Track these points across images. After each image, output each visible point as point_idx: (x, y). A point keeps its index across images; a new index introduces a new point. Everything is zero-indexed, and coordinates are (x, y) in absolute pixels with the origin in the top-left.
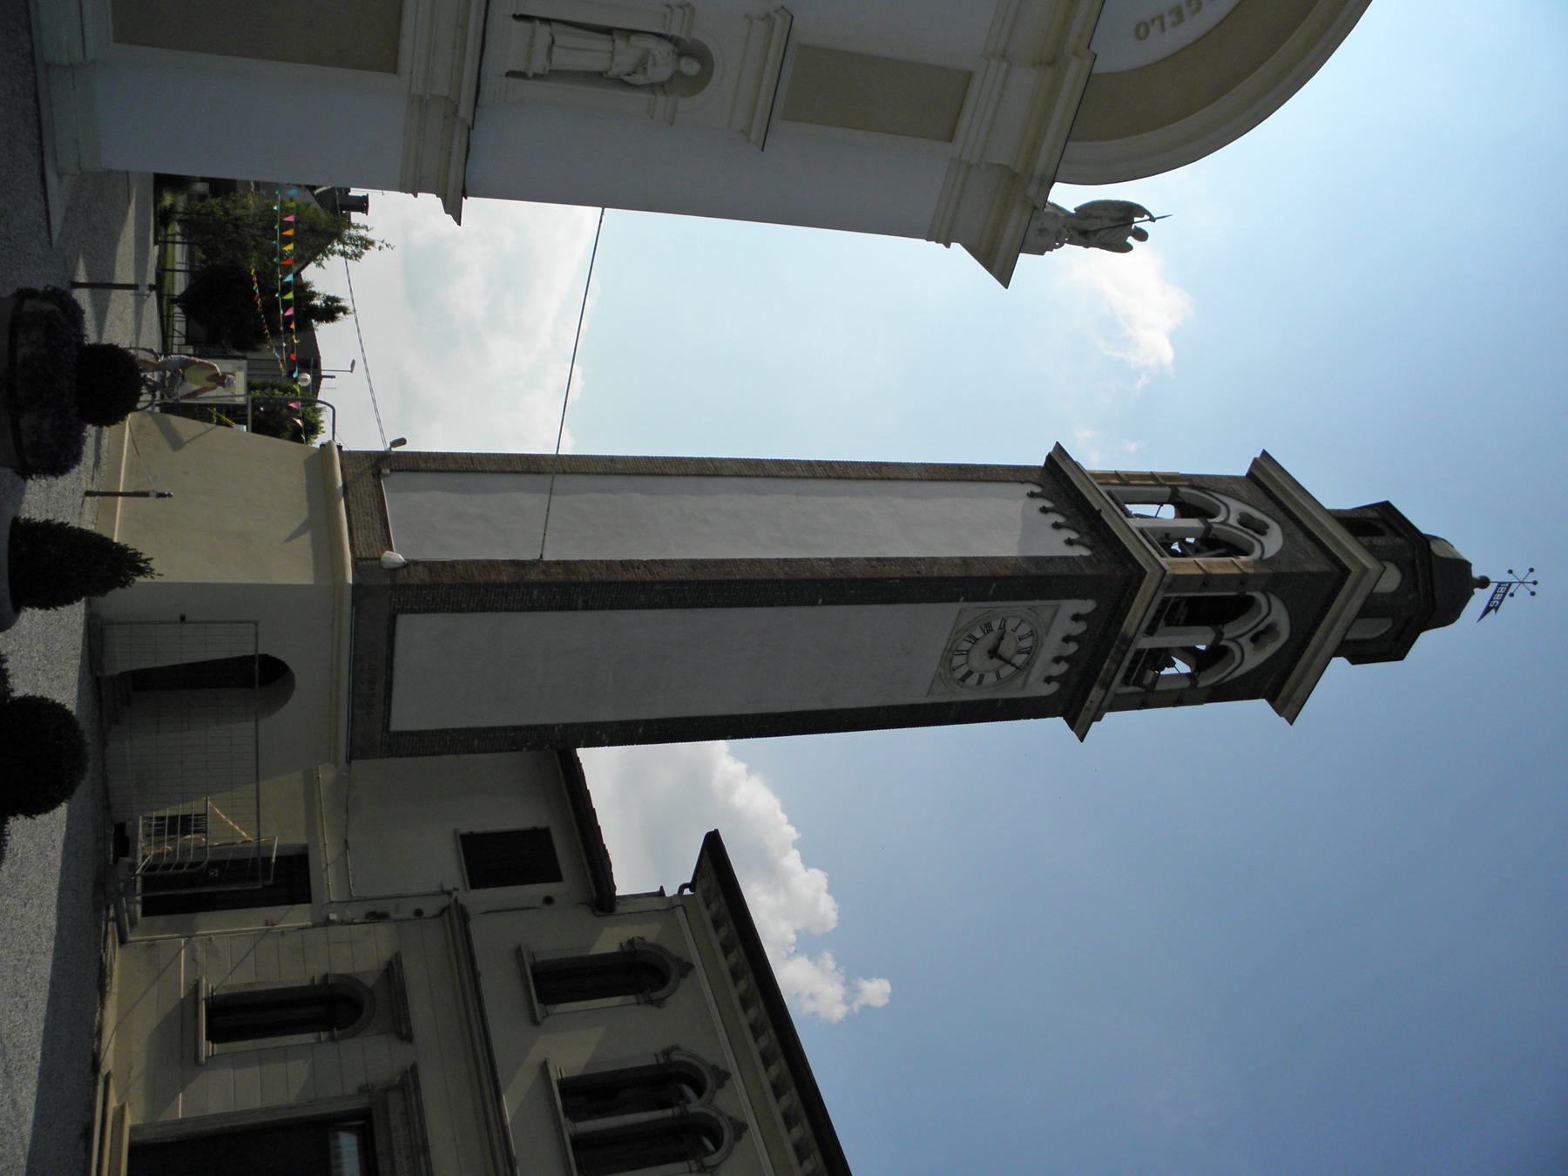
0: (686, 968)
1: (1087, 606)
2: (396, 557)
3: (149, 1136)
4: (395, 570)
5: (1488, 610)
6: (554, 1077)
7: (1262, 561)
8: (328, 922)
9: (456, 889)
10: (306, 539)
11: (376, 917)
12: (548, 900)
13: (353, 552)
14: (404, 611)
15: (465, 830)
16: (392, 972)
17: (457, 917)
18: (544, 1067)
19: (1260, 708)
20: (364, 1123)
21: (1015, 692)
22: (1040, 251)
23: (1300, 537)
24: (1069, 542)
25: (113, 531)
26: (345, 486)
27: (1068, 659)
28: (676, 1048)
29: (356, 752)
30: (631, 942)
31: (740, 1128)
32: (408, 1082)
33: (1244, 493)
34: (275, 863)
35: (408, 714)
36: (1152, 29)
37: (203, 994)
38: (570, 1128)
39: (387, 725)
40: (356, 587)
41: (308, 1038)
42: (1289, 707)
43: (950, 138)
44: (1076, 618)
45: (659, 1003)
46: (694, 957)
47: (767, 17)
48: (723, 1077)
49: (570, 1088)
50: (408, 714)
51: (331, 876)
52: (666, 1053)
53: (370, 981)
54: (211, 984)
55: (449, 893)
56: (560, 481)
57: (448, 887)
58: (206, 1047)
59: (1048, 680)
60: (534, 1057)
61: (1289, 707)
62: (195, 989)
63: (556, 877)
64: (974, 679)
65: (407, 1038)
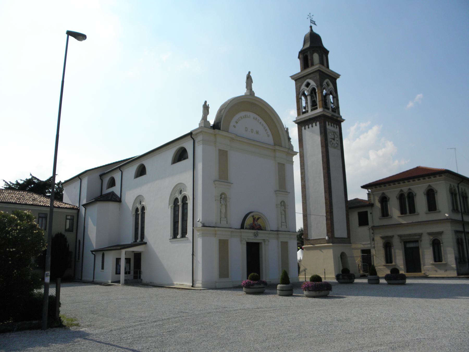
0: (383, 193)
1: (327, 123)
2: (327, 238)
3: (405, 271)
4: (329, 238)
5: (315, 24)
6: (400, 215)
7: (317, 87)
8: (374, 247)
9: (369, 227)
10: (323, 250)
11: (373, 240)
12: (371, 213)
13: (326, 244)
14: (334, 236)
15: (358, 225)
16: (382, 238)
17: (374, 228)
18: (399, 217)
19: (338, 81)
20: (405, 243)
21: (338, 134)
22: (293, 147)
23: (311, 76)
24: (316, 125)
25: (309, 277)
26: (312, 245)
27: (334, 125)
28: (397, 197)
29: (350, 243)
30: (379, 201)
31: (410, 189)
32: (400, 236)
33: (300, 84)
34: (367, 254)
35: (345, 236)
36: (268, 134)
37: (385, 264)
38: (408, 214)
39: (347, 238)
40: (332, 243)
41: (393, 250)
42: (338, 76)
43: (284, 164)
44: (329, 125)
45: (389, 198)
46: (382, 192)
47: (276, 194)
48: (401, 190)
49: (402, 213)
50: (345, 236)
51: (366, 246)
52: (397, 198)
53: (384, 241)
54: (432, 262)
55: (369, 228)
56: (308, 212)
57: (368, 229)
58: (443, 262)
59: (337, 128)
60: (397, 218)
61: (338, 76)
62: (384, 266)
63: (367, 212)
64: (337, 142)
65: (393, 236)
